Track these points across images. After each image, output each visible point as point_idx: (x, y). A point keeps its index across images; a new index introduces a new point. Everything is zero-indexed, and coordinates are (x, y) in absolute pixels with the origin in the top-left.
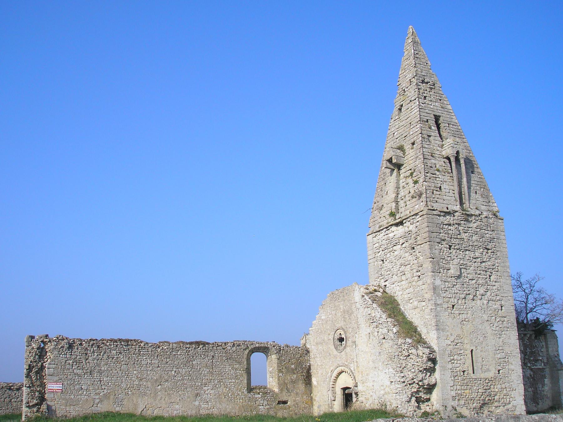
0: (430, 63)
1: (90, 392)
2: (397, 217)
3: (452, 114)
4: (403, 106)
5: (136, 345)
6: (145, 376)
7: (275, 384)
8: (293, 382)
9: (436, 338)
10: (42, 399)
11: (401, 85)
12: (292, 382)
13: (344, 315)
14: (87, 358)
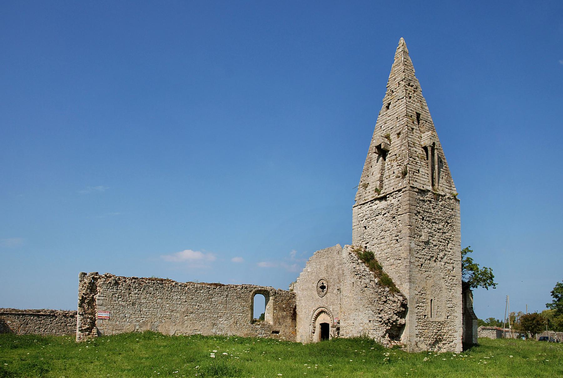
0: (415, 70)
1: (132, 320)
2: (381, 193)
3: (428, 114)
4: (391, 104)
5: (169, 284)
6: (175, 308)
7: (271, 319)
8: (283, 317)
9: (408, 289)
10: (93, 324)
11: (390, 87)
12: (283, 317)
13: (327, 269)
14: (130, 292)
